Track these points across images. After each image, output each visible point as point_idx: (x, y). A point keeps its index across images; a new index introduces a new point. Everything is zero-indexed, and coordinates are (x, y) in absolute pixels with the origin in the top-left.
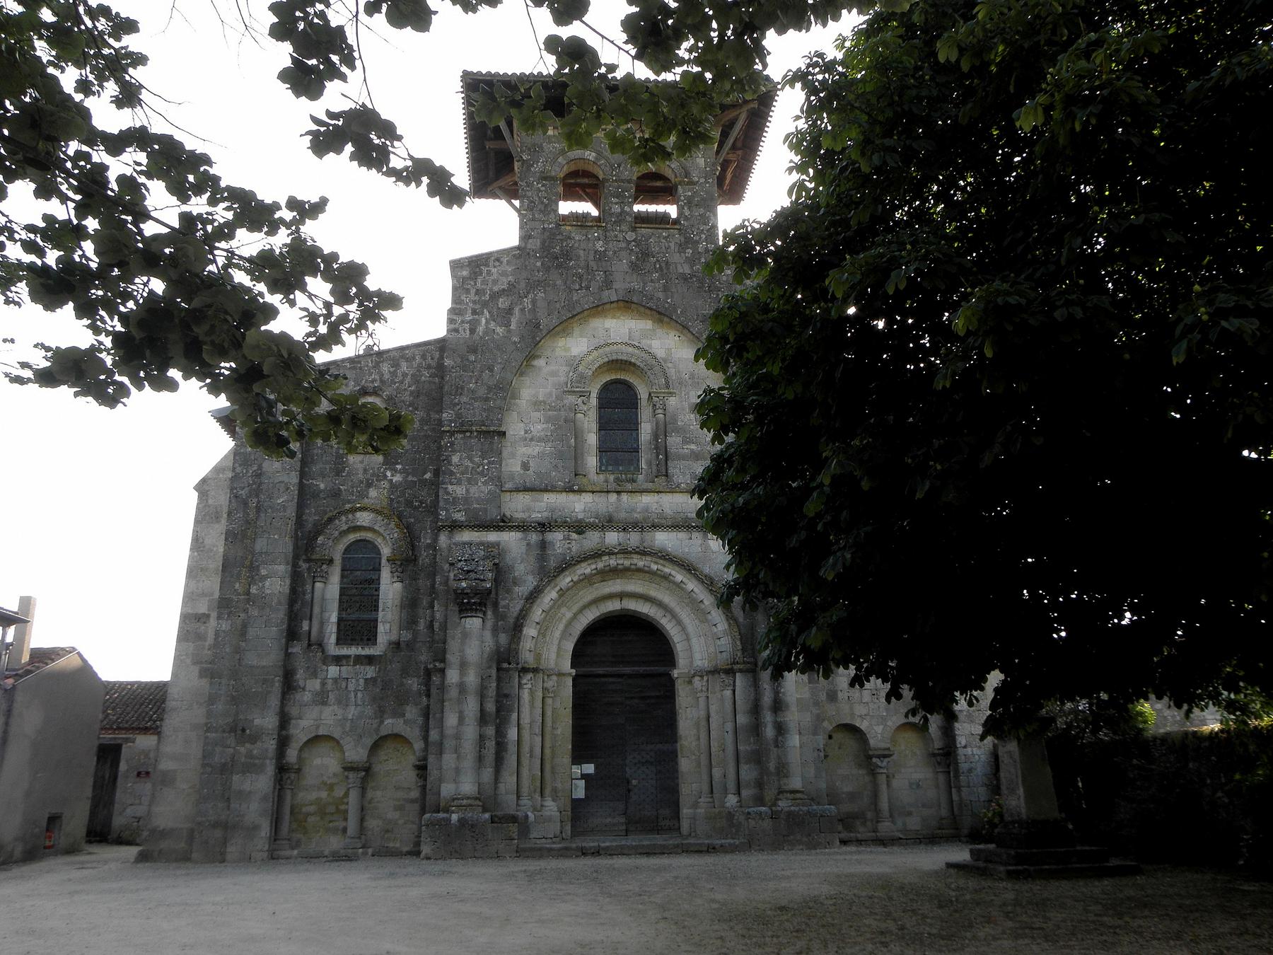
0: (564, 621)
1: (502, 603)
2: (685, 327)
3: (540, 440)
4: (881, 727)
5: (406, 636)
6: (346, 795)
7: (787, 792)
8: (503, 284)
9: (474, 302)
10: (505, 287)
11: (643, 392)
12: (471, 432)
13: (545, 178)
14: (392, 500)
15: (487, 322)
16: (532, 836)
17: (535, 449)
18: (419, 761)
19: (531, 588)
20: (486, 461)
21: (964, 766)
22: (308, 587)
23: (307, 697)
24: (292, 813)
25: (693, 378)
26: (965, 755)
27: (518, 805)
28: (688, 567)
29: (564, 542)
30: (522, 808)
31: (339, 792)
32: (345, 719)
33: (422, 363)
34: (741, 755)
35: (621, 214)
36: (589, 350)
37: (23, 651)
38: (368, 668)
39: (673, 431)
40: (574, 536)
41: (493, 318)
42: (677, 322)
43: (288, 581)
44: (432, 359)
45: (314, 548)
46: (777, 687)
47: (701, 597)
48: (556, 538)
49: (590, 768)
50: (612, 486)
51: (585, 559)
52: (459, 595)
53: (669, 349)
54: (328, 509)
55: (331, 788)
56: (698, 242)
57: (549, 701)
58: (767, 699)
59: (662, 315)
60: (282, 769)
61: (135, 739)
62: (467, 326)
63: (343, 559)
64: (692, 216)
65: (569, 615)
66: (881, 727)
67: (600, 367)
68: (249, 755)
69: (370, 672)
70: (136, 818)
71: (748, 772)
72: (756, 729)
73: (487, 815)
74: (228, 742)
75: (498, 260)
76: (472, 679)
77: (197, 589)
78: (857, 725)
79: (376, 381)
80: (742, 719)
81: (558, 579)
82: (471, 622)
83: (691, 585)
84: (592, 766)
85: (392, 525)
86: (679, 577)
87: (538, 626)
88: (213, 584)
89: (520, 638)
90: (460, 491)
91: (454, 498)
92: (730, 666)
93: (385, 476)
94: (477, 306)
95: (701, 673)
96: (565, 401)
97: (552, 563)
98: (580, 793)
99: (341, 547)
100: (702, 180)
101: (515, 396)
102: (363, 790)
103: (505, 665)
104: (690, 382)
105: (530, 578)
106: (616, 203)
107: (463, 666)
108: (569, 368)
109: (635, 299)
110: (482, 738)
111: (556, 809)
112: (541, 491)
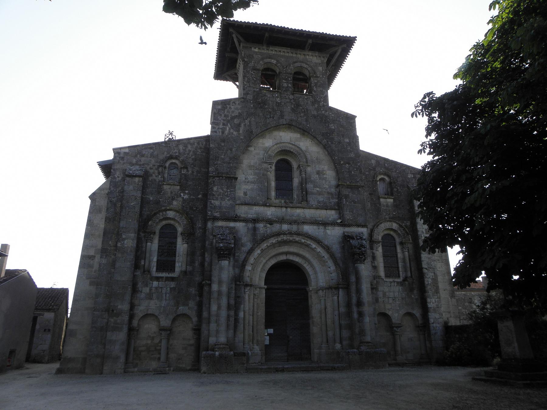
0: (262, 264)
1: (237, 254)
2: (315, 137)
3: (252, 182)
4: (397, 314)
5: (189, 268)
6: (160, 342)
7: (364, 342)
8: (236, 113)
9: (224, 120)
10: (237, 114)
11: (295, 165)
12: (222, 177)
13: (255, 69)
14: (183, 206)
15: (229, 129)
16: (250, 362)
17: (249, 187)
18: (195, 326)
19: (249, 248)
20: (229, 190)
21: (433, 332)
22: (144, 245)
23: (143, 295)
24: (134, 351)
26: (433, 327)
27: (244, 348)
28: (318, 242)
30: (245, 349)
31: (156, 341)
33: (197, 146)
35: (287, 87)
36: (273, 144)
37: (2, 270)
38: (171, 283)
39: (309, 182)
40: (268, 225)
41: (232, 127)
42: (311, 135)
43: (135, 242)
44: (202, 145)
45: (147, 227)
46: (359, 295)
47: (323, 255)
48: (260, 226)
49: (271, 331)
50: (284, 205)
51: (273, 236)
52: (218, 250)
53: (307, 147)
54: (154, 209)
55: (153, 338)
56: (320, 102)
57: (256, 300)
58: (354, 300)
59: (305, 132)
60: (131, 330)
61: (44, 314)
62: (220, 130)
63: (160, 232)
64: (317, 91)
65: (264, 261)
66: (397, 314)
67: (277, 152)
69: (173, 284)
70: (43, 350)
71: (346, 334)
72: (349, 314)
73: (232, 353)
75: (234, 102)
76: (224, 289)
77: (90, 244)
79: (177, 153)
80: (343, 310)
81: (261, 245)
82: (224, 262)
83: (319, 249)
84: (272, 330)
85: (183, 218)
86: (314, 246)
87: (252, 266)
88: (98, 243)
89: (244, 271)
90: (217, 203)
91: (214, 206)
92: (337, 286)
93: (181, 196)
94: (225, 122)
95: (322, 289)
96: (263, 166)
97: (259, 238)
98: (267, 342)
99: (159, 227)
100: (321, 76)
102: (168, 340)
103: (238, 283)
106: (285, 83)
107: (220, 282)
108: (264, 152)
109: (294, 124)
110: (228, 316)
111: (259, 350)
112: (253, 205)
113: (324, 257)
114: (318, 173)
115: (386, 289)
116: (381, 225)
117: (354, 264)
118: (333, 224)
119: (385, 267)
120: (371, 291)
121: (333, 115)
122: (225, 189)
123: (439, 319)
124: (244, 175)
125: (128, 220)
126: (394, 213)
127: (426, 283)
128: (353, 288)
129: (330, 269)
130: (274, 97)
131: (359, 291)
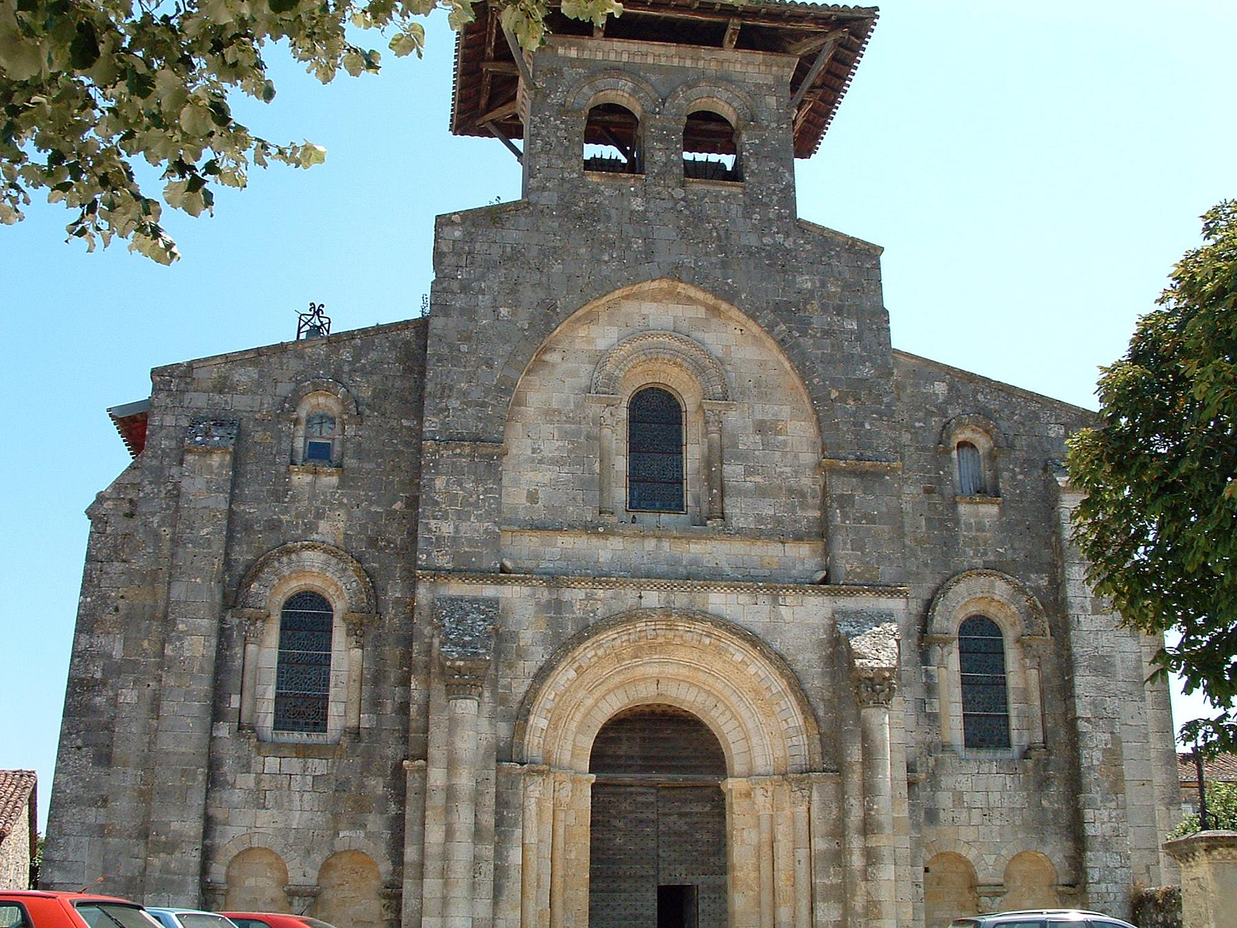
1: (502, 682)
4: (994, 857)
5: (366, 721)
13: (566, 112)
17: (545, 475)
22: (238, 650)
23: (237, 796)
25: (760, 387)
29: (586, 602)
32: (288, 828)
43: (214, 641)
57: (561, 816)
63: (284, 615)
66: (994, 857)
68: (166, 869)
74: (136, 850)
76: (464, 781)
82: (464, 706)
90: (447, 528)
97: (570, 630)
99: (280, 599)
101: (519, 402)
104: (755, 391)
105: (540, 649)
107: (452, 765)
110: (477, 860)
114: (762, 428)
115: (964, 783)
116: (955, 588)
118: (804, 585)
121: (808, 247)
122: (469, 486)
123: (1117, 871)
124: (530, 441)
125: (193, 580)
126: (1000, 550)
127: (1085, 763)
128: (855, 778)
130: (622, 194)
131: (869, 790)
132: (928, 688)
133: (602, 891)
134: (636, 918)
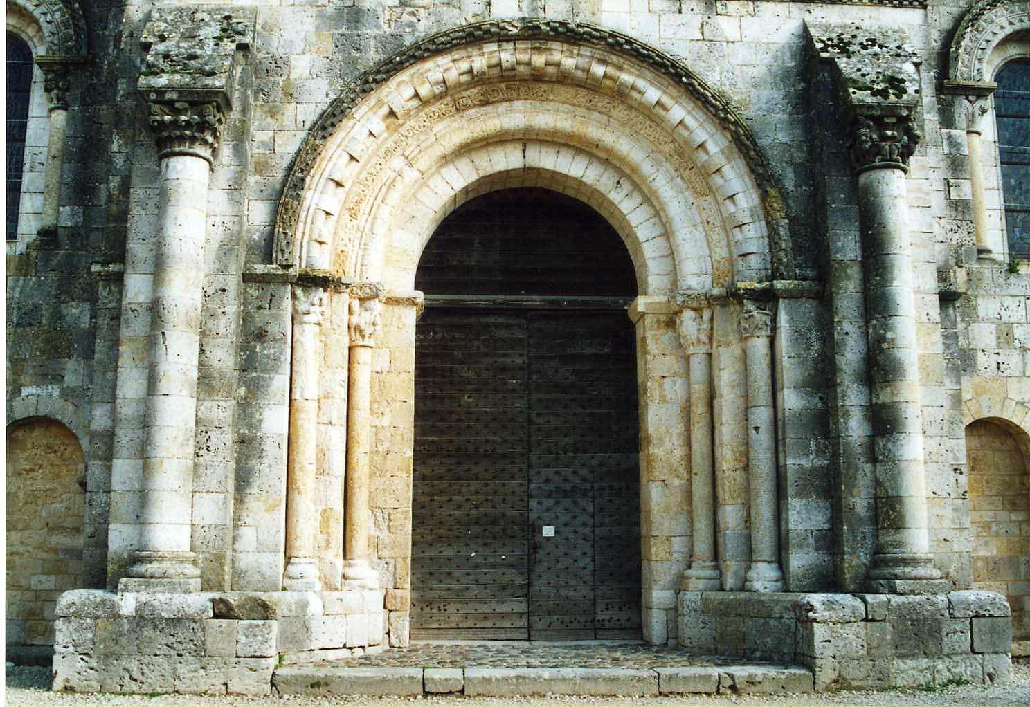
29: (399, 10)
34: (791, 476)
58: (850, 356)
78: (1015, 421)
83: (679, 111)
84: (544, 534)
97: (373, 56)
113: (702, 146)
117: (856, 175)
119: (1008, 211)
120: (938, 310)
128: (848, 292)
129: (734, 202)
132: (953, 163)
133: (440, 478)
134: (494, 522)
